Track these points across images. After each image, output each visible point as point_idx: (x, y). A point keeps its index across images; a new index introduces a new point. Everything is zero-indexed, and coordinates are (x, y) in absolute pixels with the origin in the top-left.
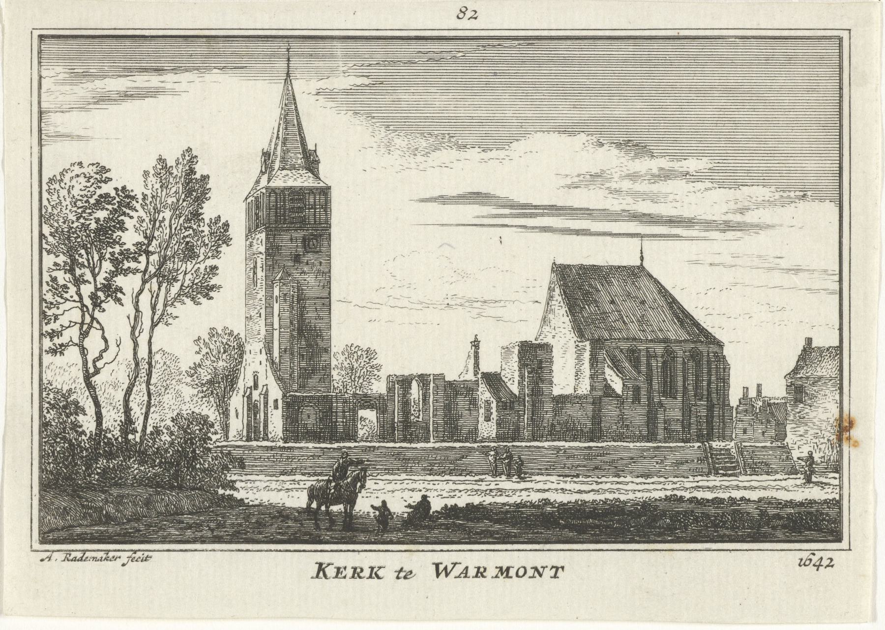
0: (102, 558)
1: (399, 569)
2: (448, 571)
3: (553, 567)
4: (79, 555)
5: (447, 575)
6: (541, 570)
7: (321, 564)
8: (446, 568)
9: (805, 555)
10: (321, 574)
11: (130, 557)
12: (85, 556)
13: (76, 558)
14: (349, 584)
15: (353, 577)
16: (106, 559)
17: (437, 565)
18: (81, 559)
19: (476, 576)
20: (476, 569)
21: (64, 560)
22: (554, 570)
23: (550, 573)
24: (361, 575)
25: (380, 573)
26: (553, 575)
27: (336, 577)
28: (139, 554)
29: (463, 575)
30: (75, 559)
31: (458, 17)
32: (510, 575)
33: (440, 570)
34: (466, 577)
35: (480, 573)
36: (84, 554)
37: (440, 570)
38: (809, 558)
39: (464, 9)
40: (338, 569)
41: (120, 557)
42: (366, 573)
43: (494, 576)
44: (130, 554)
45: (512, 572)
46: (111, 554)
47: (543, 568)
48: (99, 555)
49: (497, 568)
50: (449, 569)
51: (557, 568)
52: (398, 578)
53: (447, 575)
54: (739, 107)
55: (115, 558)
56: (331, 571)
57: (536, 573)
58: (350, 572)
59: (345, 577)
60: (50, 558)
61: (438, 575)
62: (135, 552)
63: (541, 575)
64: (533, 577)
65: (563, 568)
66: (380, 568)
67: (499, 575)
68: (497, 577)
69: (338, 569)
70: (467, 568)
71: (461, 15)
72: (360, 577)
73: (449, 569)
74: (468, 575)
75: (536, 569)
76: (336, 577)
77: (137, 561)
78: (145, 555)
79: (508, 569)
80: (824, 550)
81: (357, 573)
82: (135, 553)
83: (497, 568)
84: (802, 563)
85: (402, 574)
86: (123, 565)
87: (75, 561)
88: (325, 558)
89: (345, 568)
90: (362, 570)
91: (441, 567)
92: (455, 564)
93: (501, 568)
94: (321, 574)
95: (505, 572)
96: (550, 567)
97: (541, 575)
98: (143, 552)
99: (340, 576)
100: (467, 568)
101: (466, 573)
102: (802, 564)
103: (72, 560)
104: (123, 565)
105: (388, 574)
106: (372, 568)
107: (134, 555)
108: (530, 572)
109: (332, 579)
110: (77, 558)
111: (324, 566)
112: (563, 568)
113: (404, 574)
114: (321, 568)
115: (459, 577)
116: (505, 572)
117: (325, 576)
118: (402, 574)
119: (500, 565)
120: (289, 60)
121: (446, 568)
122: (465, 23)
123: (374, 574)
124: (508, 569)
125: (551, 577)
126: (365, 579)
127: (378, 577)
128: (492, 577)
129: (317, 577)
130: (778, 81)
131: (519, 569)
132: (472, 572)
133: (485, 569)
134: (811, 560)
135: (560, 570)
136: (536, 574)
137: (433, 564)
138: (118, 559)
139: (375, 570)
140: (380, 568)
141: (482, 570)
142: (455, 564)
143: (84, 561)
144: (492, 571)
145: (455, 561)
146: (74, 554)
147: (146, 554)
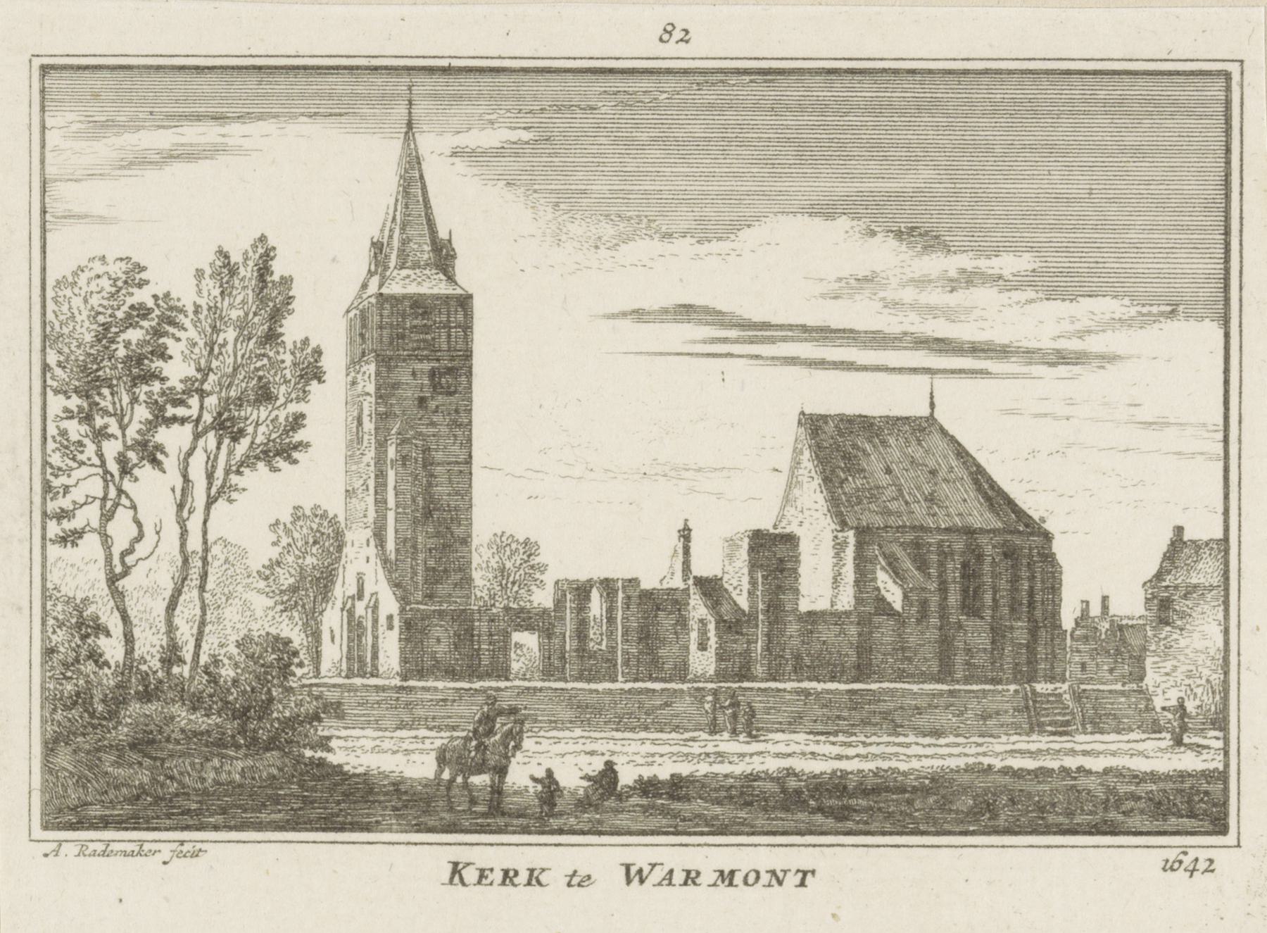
1: (571, 873)
3: (798, 871)
4: (100, 847)
5: (642, 881)
6: (781, 875)
7: (456, 864)
8: (640, 871)
9: (1172, 855)
10: (457, 879)
12: (110, 848)
14: (496, 893)
16: (139, 854)
17: (628, 868)
18: (104, 854)
19: (685, 884)
21: (79, 855)
22: (800, 875)
25: (543, 878)
26: (798, 882)
27: (479, 882)
29: (666, 882)
30: (94, 853)
31: (661, 40)
32: (735, 882)
33: (632, 875)
34: (670, 884)
35: (691, 878)
37: (83, 844)
38: (1180, 858)
39: (669, 28)
40: (482, 871)
41: (46, 855)
42: (523, 877)
45: (738, 879)
46: (146, 847)
47: (785, 872)
51: (805, 873)
52: (569, 885)
53: (642, 881)
56: (470, 875)
58: (498, 876)
59: (491, 884)
61: (629, 881)
62: (182, 843)
63: (780, 883)
64: (769, 885)
65: (813, 872)
66: (543, 870)
67: (719, 882)
68: (715, 885)
69: (482, 871)
70: (671, 872)
71: (666, 37)
72: (514, 885)
73: (645, 873)
75: (773, 873)
76: (479, 882)
77: (185, 856)
79: (732, 873)
80: (1200, 846)
81: (508, 877)
82: (1185, 853)
85: (575, 881)
86: (165, 863)
88: (462, 855)
89: (492, 870)
90: (516, 873)
91: (633, 870)
92: (653, 866)
94: (457, 879)
95: (727, 877)
96: (794, 871)
97: (780, 883)
99: (484, 881)
100: (671, 872)
101: (670, 879)
102: (1169, 867)
103: (90, 855)
104: (165, 863)
105: (555, 879)
106: (532, 871)
108: (765, 878)
111: (460, 866)
112: (813, 872)
113: (578, 880)
114: (456, 870)
115: (660, 884)
116: (727, 877)
117: (463, 884)
118: (575, 881)
119: (721, 869)
122: (671, 49)
123: (534, 878)
124: (732, 873)
131: (747, 875)
132: (679, 877)
133: (698, 873)
134: (1181, 862)
135: (809, 875)
136: (774, 882)
137: (622, 865)
139: (536, 874)
141: (511, 874)
142: (653, 866)
144: (708, 877)
145: (653, 862)
147: (199, 846)
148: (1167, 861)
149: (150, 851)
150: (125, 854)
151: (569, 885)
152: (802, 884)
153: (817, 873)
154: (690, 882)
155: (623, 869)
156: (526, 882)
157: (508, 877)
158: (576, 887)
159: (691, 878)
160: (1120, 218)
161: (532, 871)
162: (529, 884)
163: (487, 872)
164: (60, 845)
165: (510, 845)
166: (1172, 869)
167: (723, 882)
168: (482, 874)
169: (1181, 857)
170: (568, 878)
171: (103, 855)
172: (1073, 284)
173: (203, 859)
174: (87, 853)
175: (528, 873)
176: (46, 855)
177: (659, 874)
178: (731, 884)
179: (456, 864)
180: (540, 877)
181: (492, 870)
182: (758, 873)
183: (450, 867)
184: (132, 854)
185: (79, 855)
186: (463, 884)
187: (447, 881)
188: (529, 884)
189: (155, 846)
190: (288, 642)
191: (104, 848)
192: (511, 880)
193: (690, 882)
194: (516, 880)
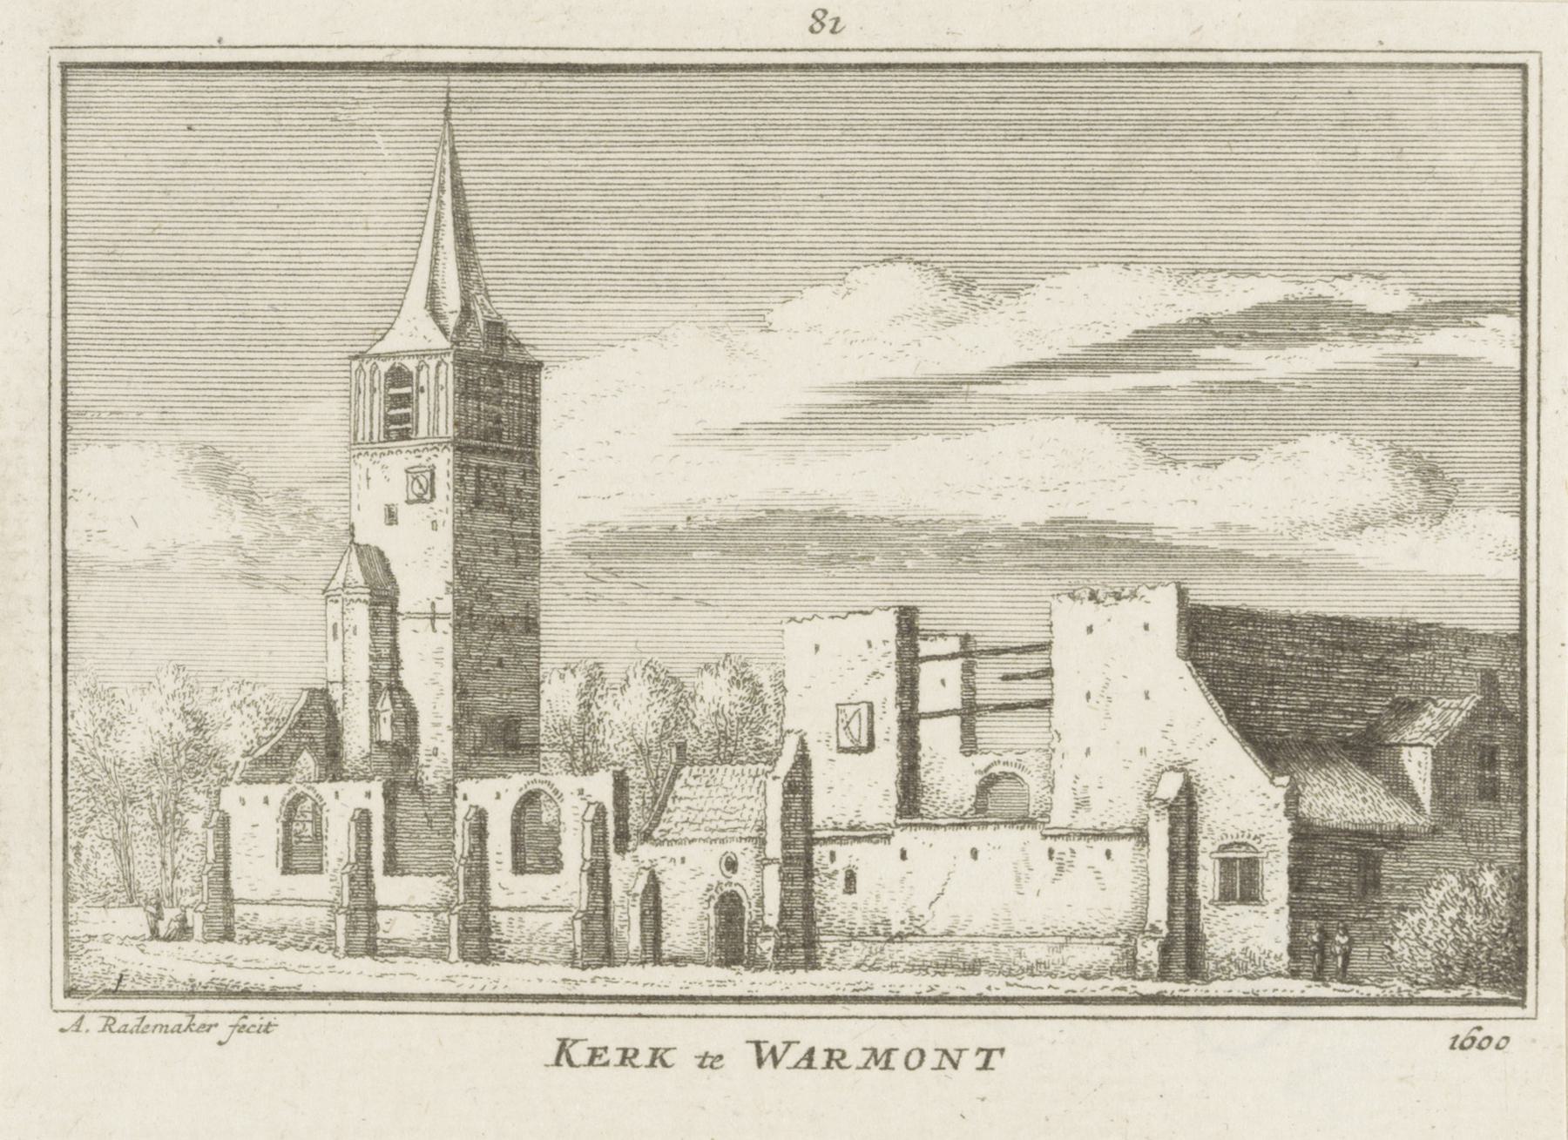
0: (180, 1026)
1: (703, 1054)
2: (779, 1056)
4: (132, 1020)
5: (776, 1063)
6: (955, 1056)
7: (563, 1041)
8: (773, 1050)
9: (1463, 1029)
10: (563, 1060)
11: (235, 1026)
12: (145, 1023)
13: (180, 1026)
14: (613, 1077)
15: (828, 1066)
17: (758, 1044)
18: (140, 1030)
20: (621, 1052)
21: (104, 1030)
22: (983, 1055)
23: (971, 1061)
24: (843, 1063)
25: (668, 1058)
26: (980, 1064)
28: (254, 1019)
29: (804, 1063)
30: (124, 1030)
31: (812, 30)
34: (810, 1066)
35: (835, 1059)
36: (143, 1018)
38: (1473, 1034)
40: (594, 1050)
41: (62, 1030)
42: (644, 1058)
43: (861, 1065)
44: (234, 1019)
45: (897, 1060)
46: (199, 1019)
48: (173, 1020)
49: (865, 1049)
50: (779, 1053)
51: (990, 1052)
53: (776, 1063)
54: (903, 192)
55: (207, 1028)
56: (580, 1054)
57: (945, 1058)
58: (615, 1057)
59: (606, 1064)
60: (77, 1027)
61: (760, 1062)
62: (246, 1014)
63: (955, 1066)
65: (1002, 1051)
66: (667, 1050)
67: (871, 1063)
68: (866, 1067)
70: (811, 1051)
72: (633, 1066)
73: (779, 1053)
74: (814, 1065)
76: (591, 1062)
77: (248, 1031)
78: (265, 1022)
79: (889, 1052)
80: (1497, 1021)
81: (627, 1057)
83: (865, 1049)
84: (1457, 1044)
85: (708, 1061)
86: (220, 1043)
87: (124, 1032)
89: (606, 1049)
90: (636, 1052)
91: (766, 1049)
92: (789, 1044)
93: (874, 1051)
95: (881, 1059)
96: (974, 1050)
97: (955, 1066)
98: (141, 1015)
99: (597, 1061)
100: (811, 1051)
104: (220, 1043)
105: (683, 1059)
107: (244, 1021)
108: (933, 1058)
109: (643, 1069)
110: (128, 1029)
112: (1002, 1051)
113: (710, 1061)
114: (563, 1047)
115: (796, 1067)
116: (881, 1059)
117: (571, 1063)
118: (708, 1061)
120: (447, 112)
121: (773, 1050)
122: (825, 39)
123: (658, 1058)
124: (889, 1052)
125: (978, 1069)
126: (643, 1069)
127: (664, 1064)
128: (858, 1068)
129: (557, 1064)
130: (214, 151)
132: (820, 1058)
134: (1474, 1039)
135: (996, 1054)
136: (946, 1063)
138: (213, 1029)
139: (660, 1052)
140: (667, 1050)
142: (789, 1044)
143: (143, 1032)
144: (856, 1057)
145: (789, 1039)
146: (121, 1019)
147: (268, 1018)
148: (1457, 1037)
149: (204, 1025)
150: (164, 1029)
151: (701, 1066)
152: (985, 1066)
153: (1006, 1053)
154: (833, 1064)
155: (752, 1047)
156: (648, 1063)
157: (627, 1057)
158: (709, 1069)
159: (835, 1059)
160: (1297, 228)
161: (656, 1050)
162: (652, 1065)
163: (599, 1052)
164: (82, 1018)
165: (728, 1017)
166: (1462, 1047)
167: (877, 1063)
168: (594, 1053)
169: (1475, 1033)
170: (699, 1060)
171: (137, 1031)
172: (284, 355)
173: (275, 1032)
174: (115, 1028)
175: (651, 1053)
176: (62, 1030)
177: (796, 1053)
178: (887, 1067)
179: (563, 1041)
180: (665, 1057)
181: (606, 1049)
182: (922, 1053)
183: (556, 1045)
184: (178, 1029)
185: (104, 1030)
186: (571, 1063)
187: (552, 1060)
188: (652, 1065)
189: (212, 1019)
190: (571, 768)
191: (138, 1022)
192: (837, 1061)
193: (657, 1062)
194: (636, 1061)
